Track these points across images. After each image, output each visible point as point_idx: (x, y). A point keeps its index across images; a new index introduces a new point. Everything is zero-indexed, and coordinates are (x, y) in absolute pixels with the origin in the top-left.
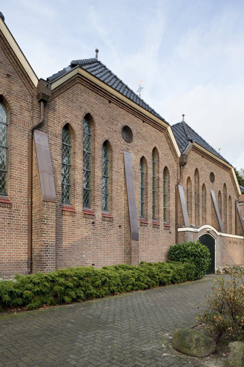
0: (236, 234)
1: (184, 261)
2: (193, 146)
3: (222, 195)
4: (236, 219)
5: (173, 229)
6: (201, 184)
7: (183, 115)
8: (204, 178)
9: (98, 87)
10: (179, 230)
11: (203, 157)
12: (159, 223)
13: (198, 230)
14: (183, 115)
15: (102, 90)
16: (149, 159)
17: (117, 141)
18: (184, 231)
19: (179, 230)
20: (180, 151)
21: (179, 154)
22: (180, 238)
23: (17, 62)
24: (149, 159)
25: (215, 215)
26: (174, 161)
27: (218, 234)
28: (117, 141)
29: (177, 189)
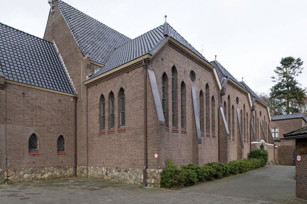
0: (269, 143)
1: (259, 158)
2: (228, 80)
3: (204, 96)
4: (218, 119)
5: (249, 142)
6: (231, 106)
7: (243, 78)
8: (233, 102)
9: (176, 46)
10: (252, 143)
11: (233, 87)
12: (178, 129)
13: (260, 143)
14: (243, 78)
15: (179, 47)
16: (170, 75)
17: (188, 81)
18: (255, 144)
19: (252, 143)
20: (221, 84)
21: (252, 105)
22: (253, 147)
23: (216, 80)
24: (170, 75)
25: (263, 134)
26: (249, 109)
27: (266, 144)
28: (188, 81)
29: (219, 110)
